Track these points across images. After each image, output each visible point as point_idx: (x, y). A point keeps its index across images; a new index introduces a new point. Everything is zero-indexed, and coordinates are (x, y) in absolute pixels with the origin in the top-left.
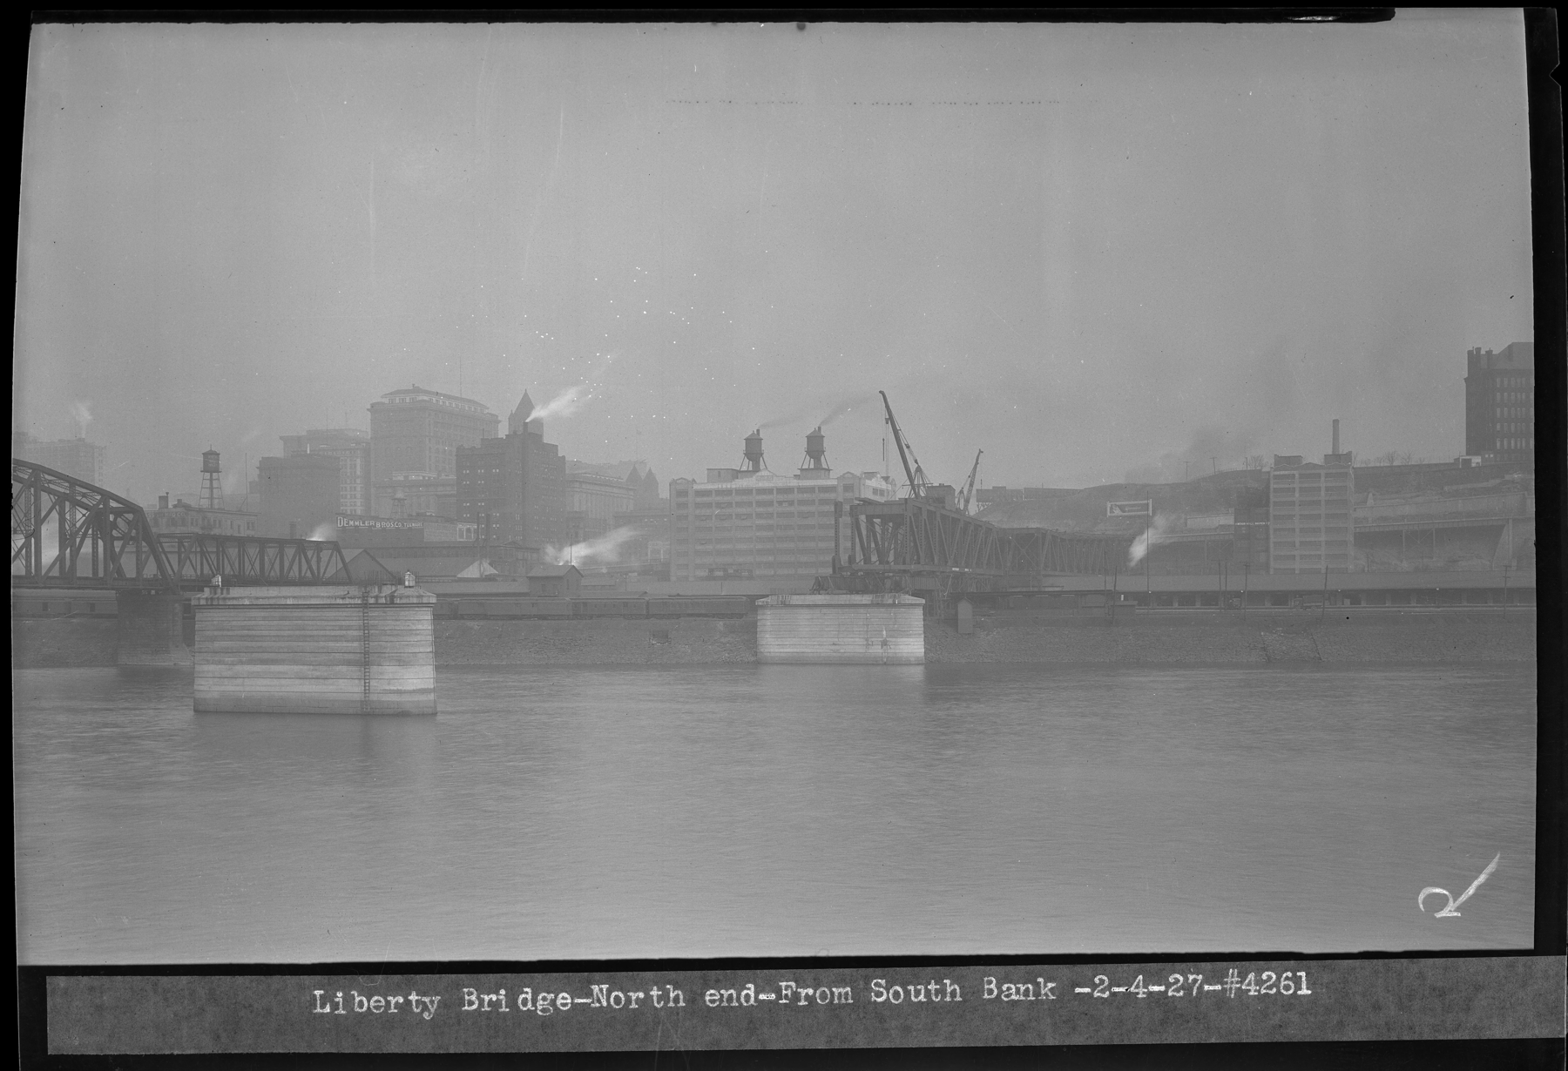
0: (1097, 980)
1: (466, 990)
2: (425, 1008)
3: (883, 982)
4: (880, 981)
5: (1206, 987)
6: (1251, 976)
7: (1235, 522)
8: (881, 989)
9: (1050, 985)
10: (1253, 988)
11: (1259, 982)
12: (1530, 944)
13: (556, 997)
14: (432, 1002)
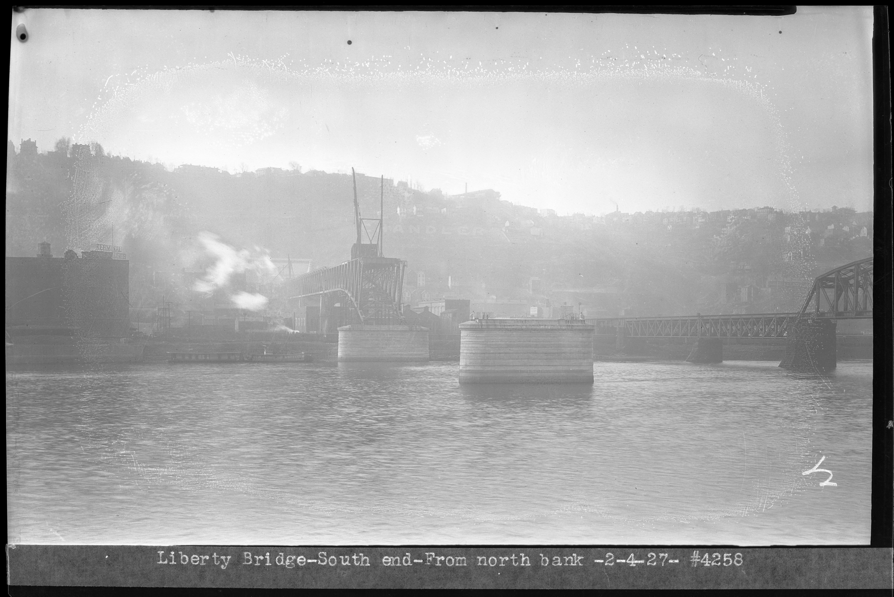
2: (222, 563)
3: (325, 554)
4: (323, 553)
5: (671, 561)
6: (707, 555)
8: (447, 559)
9: (580, 558)
11: (711, 559)
12: (869, 543)
13: (297, 558)
14: (226, 559)
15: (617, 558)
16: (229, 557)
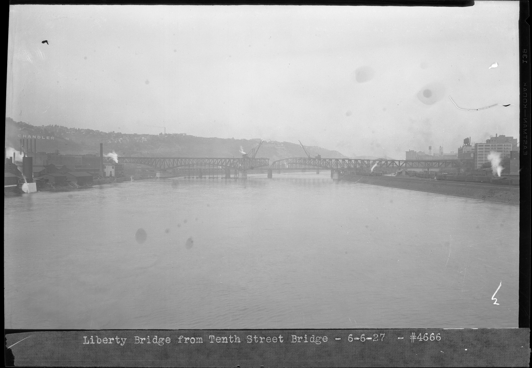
0: (374, 335)
1: (136, 337)
7: (34, 173)
10: (421, 338)
13: (266, 338)
15: (366, 337)
16: (125, 339)
